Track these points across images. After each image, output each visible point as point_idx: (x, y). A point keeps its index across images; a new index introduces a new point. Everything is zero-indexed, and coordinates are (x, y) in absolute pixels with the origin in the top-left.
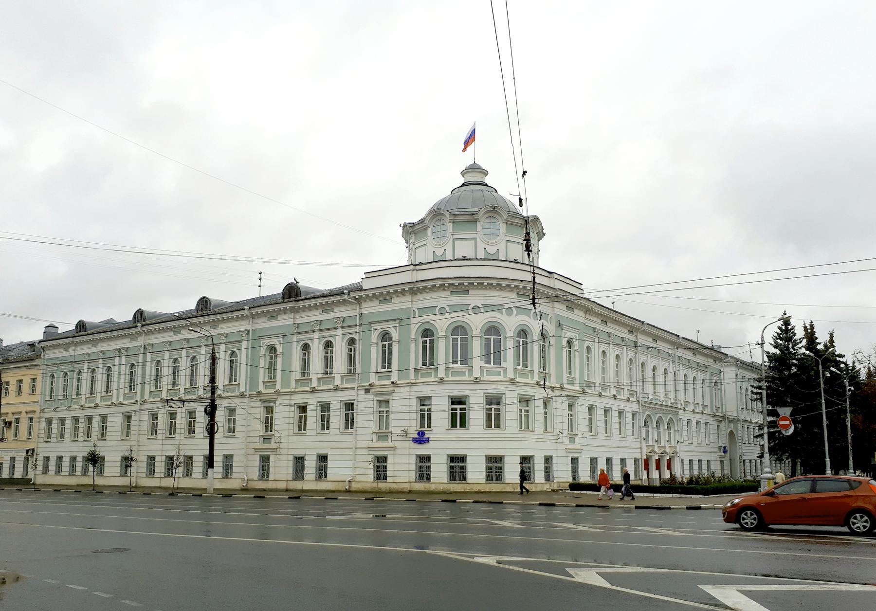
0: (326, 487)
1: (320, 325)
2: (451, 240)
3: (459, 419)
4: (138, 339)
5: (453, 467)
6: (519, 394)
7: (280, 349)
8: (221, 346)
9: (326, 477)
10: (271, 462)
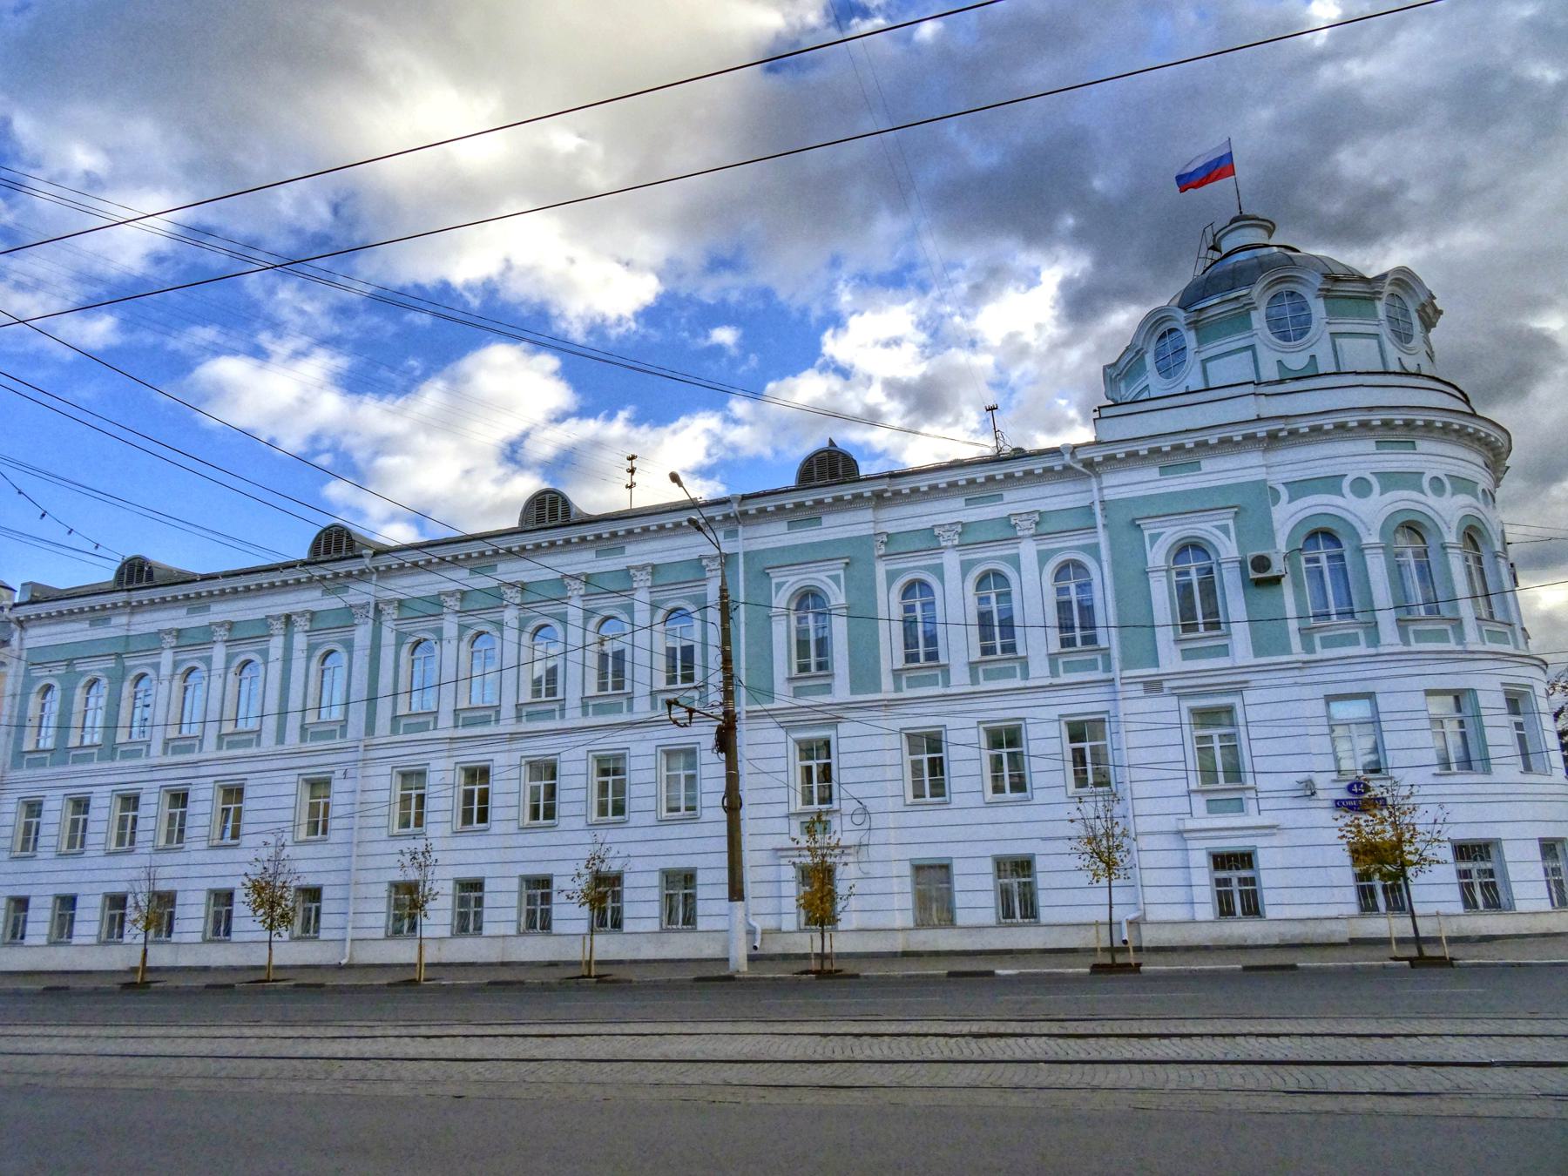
0: (1045, 943)
1: (311, 621)
2: (1327, 336)
3: (476, 810)
4: (212, 609)
5: (1465, 871)
6: (1503, 684)
7: (837, 597)
8: (356, 632)
9: (479, 928)
10: (698, 887)
